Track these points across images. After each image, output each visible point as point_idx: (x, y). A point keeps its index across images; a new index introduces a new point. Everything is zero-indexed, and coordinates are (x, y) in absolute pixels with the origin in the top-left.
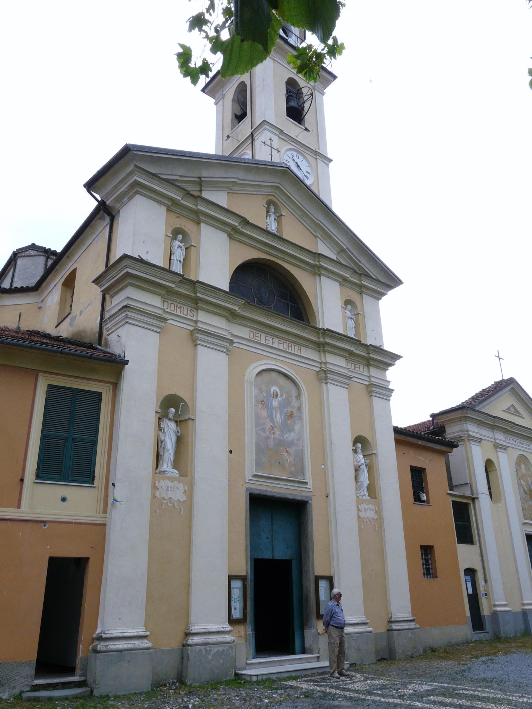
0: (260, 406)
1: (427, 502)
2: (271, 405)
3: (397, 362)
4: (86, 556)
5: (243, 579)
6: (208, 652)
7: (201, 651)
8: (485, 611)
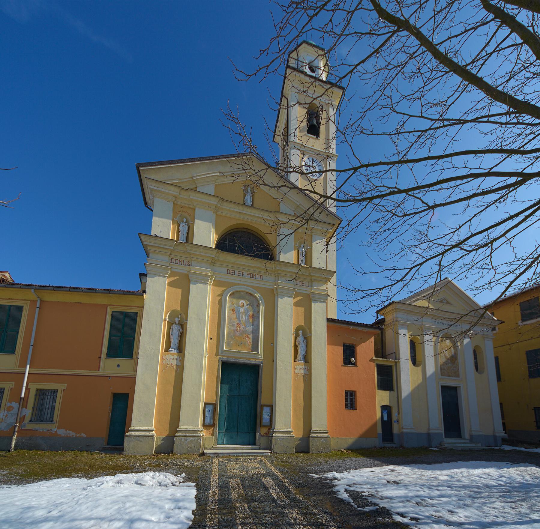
0: (232, 312)
1: (354, 364)
2: (239, 311)
5: (214, 405)
7: (182, 439)
8: (396, 429)
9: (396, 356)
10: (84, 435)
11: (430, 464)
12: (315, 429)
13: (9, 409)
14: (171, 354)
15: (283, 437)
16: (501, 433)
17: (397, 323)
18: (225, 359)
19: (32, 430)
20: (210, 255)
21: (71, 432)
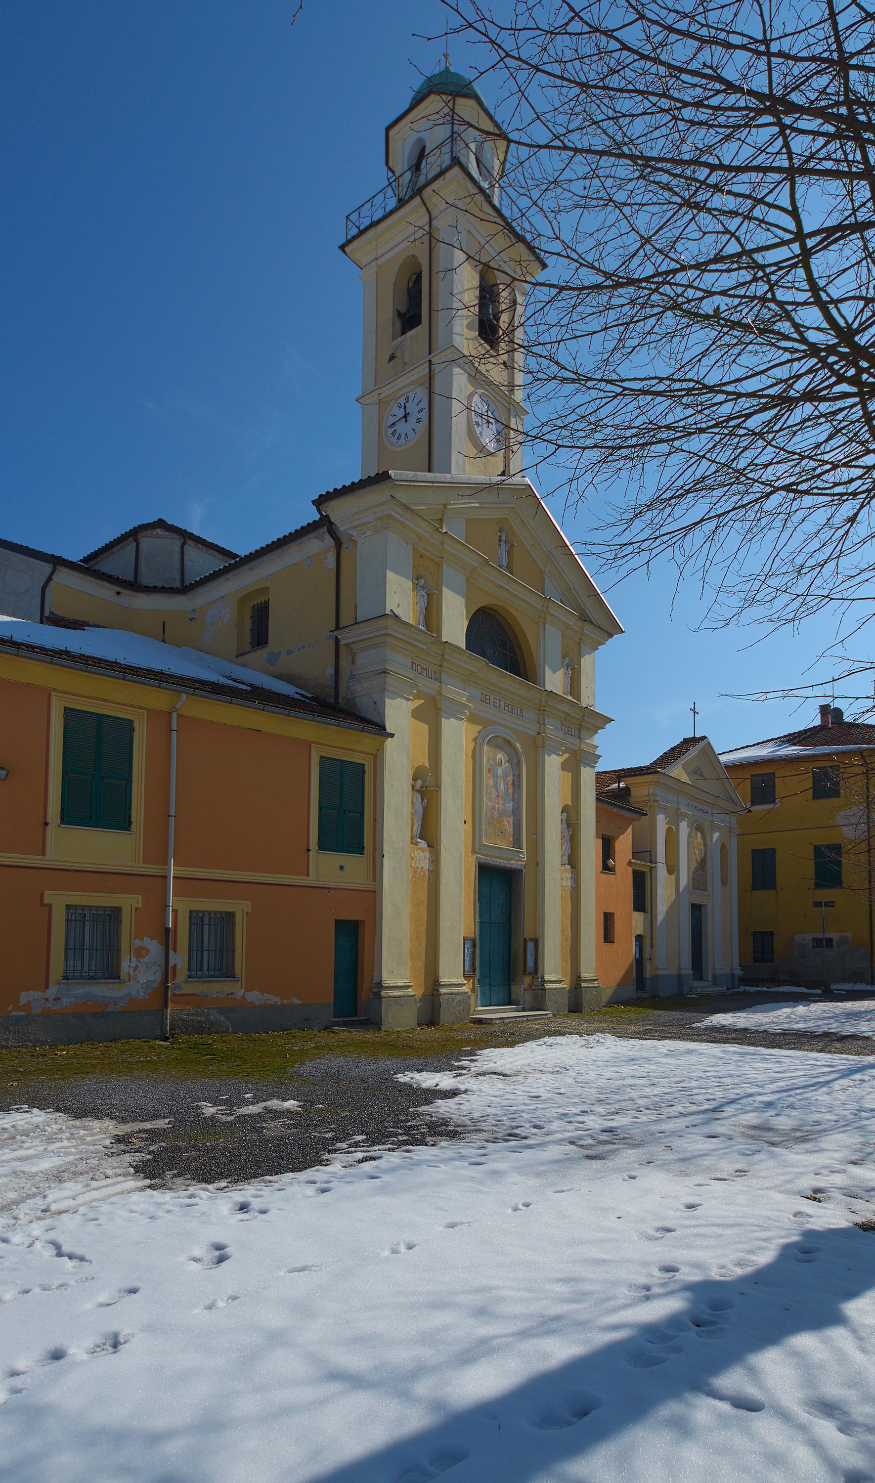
3: (608, 726)
4: (356, 919)
6: (453, 1000)
8: (648, 974)
9: (652, 860)
10: (297, 1001)
11: (511, 1045)
12: (586, 975)
13: (140, 952)
14: (420, 849)
15: (555, 989)
16: (738, 972)
17: (655, 804)
18: (485, 859)
19: (195, 995)
20: (469, 667)
21: (270, 996)
